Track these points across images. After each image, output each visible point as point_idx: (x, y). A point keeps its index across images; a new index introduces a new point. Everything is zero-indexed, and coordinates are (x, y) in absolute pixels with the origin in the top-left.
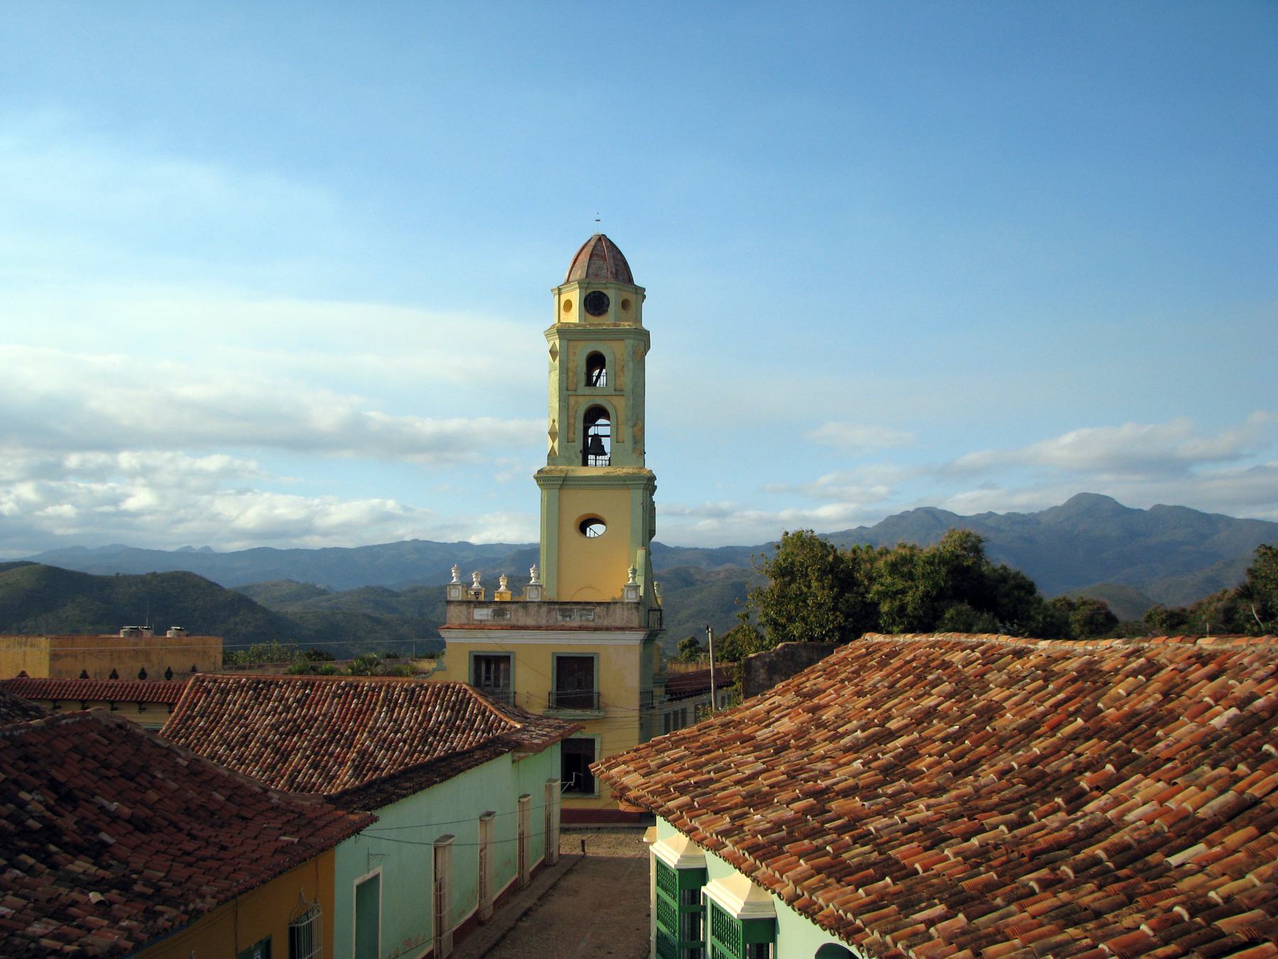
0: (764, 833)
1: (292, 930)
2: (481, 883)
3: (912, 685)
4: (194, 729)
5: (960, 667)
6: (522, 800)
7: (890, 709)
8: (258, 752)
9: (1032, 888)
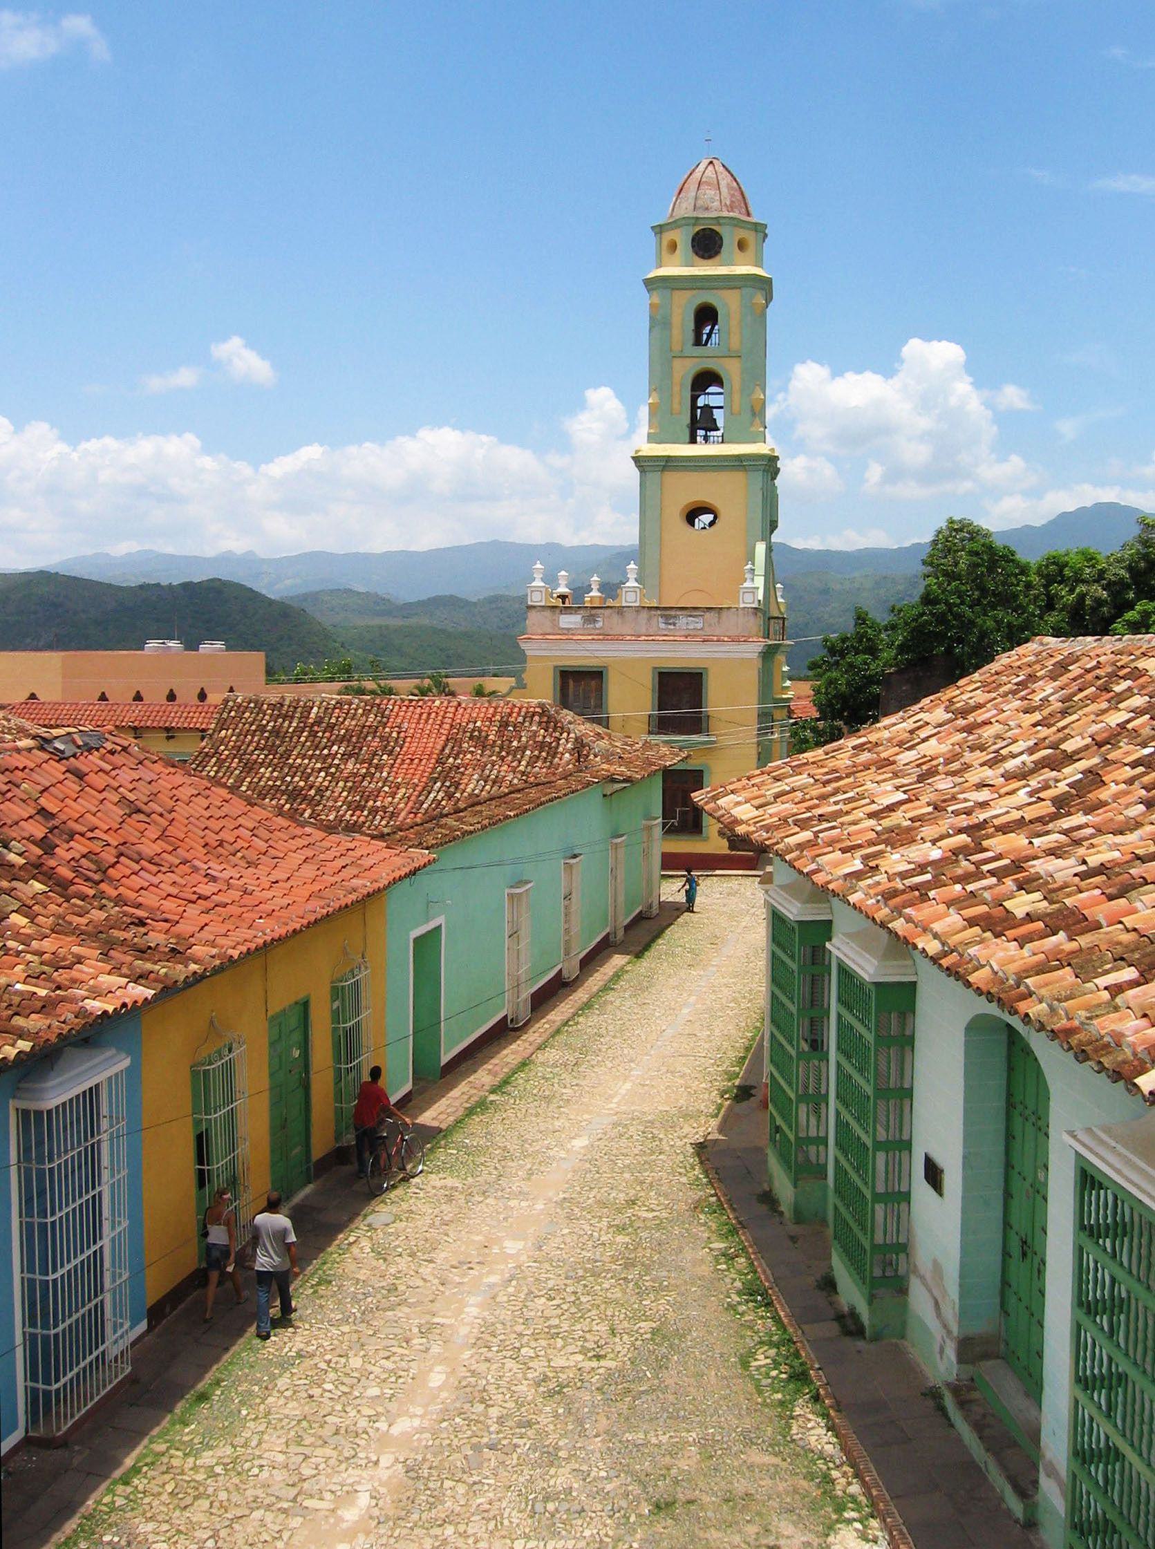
0: (904, 875)
3: (1093, 699)
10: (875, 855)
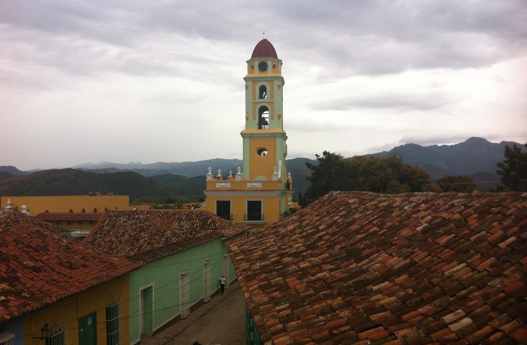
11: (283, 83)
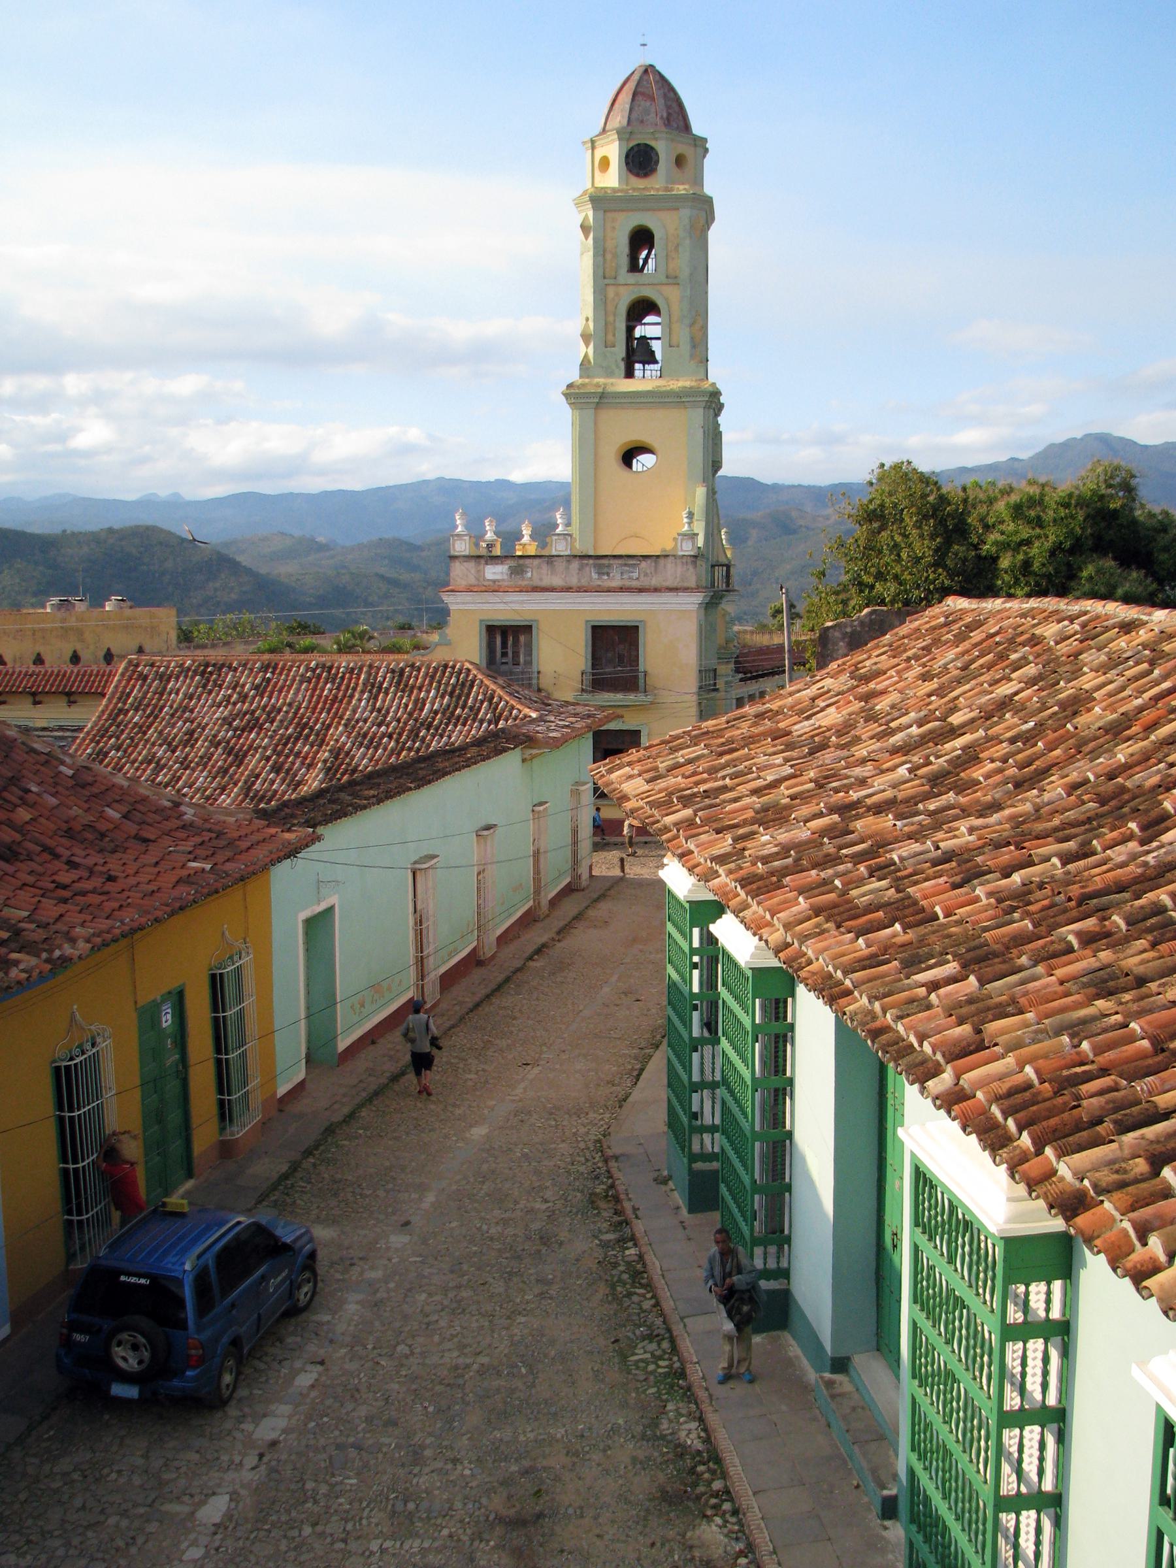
0: (766, 860)
1: (213, 976)
2: (479, 914)
3: (989, 667)
4: (126, 726)
5: (1052, 643)
6: (537, 809)
7: (957, 698)
8: (206, 754)
9: (1069, 944)
10: (744, 837)
11: (710, 218)
